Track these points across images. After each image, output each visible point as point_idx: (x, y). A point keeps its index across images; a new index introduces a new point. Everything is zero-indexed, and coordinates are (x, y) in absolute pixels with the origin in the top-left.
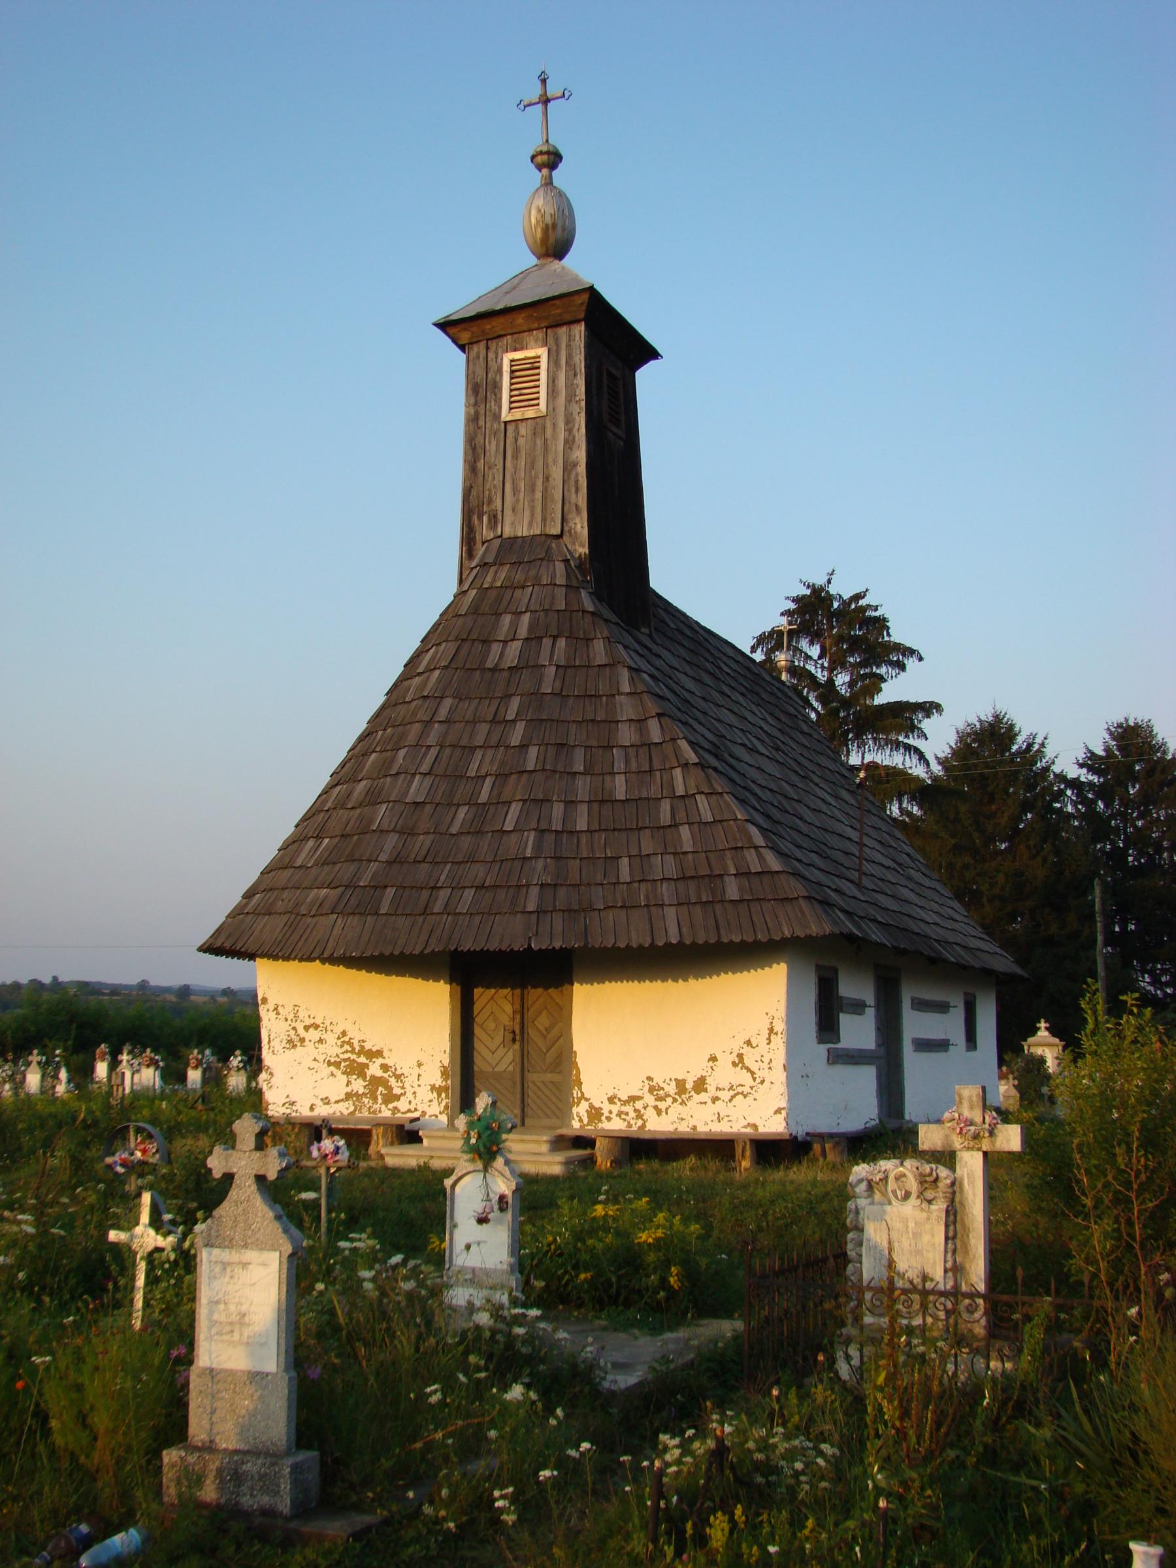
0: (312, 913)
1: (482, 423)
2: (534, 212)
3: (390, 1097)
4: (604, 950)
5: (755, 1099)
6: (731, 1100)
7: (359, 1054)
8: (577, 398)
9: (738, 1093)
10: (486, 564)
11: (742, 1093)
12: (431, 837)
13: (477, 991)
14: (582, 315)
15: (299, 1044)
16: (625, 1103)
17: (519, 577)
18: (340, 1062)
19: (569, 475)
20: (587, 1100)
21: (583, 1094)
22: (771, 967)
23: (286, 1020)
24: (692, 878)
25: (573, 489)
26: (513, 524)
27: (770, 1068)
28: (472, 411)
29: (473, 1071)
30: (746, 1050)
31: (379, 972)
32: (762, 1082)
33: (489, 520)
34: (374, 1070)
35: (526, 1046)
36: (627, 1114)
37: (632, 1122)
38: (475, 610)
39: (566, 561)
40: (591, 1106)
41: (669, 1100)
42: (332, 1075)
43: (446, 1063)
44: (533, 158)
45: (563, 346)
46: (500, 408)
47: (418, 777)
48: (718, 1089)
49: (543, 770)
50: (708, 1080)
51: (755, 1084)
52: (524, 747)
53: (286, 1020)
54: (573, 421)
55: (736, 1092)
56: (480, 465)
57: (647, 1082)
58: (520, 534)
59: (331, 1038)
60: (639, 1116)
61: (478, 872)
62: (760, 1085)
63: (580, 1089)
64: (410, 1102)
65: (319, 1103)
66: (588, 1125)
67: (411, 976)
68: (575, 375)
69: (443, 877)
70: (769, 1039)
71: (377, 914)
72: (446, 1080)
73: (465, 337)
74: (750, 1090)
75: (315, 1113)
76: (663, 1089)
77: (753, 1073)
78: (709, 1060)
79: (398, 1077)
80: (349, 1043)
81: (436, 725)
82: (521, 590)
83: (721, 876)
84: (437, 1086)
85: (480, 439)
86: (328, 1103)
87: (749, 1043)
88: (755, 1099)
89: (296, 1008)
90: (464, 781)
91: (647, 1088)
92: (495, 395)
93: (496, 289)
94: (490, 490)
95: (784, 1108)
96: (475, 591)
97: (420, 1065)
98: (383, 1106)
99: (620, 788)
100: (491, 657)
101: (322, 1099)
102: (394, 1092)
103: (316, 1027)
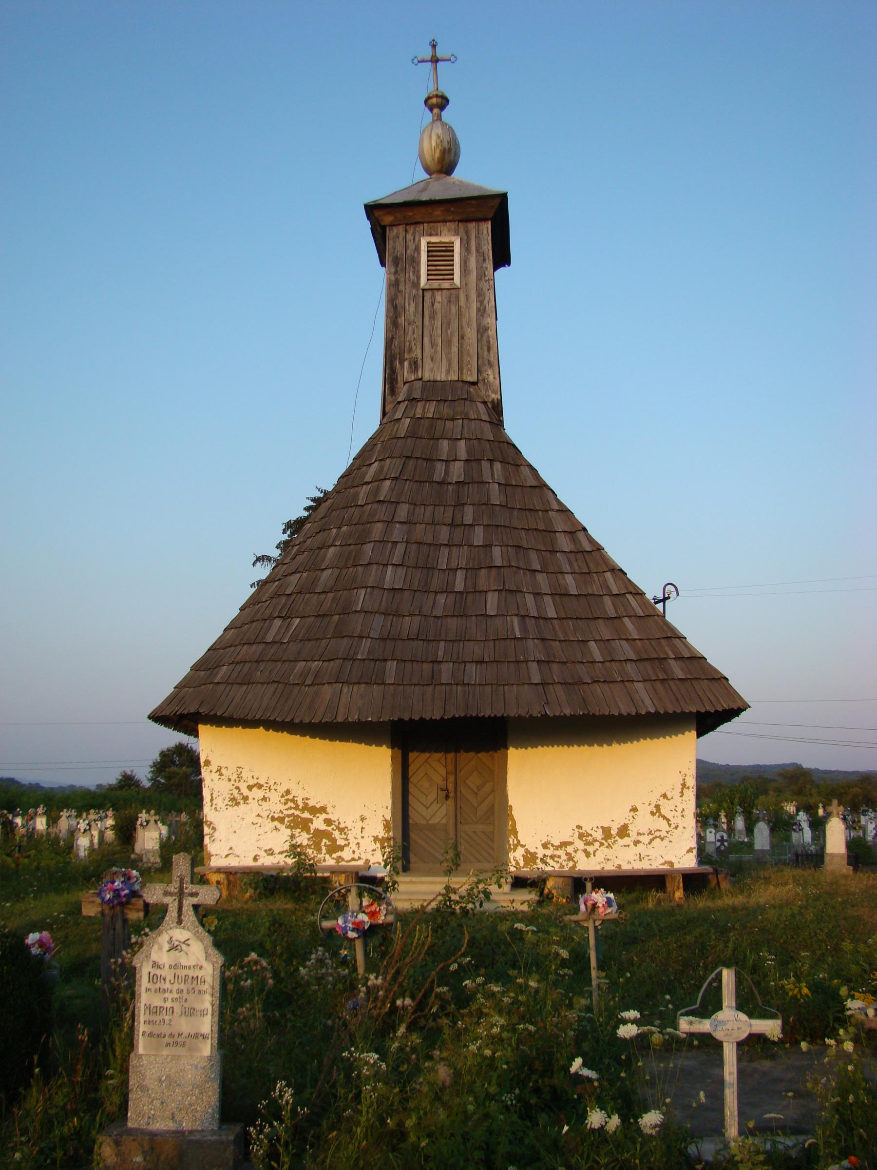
0: (308, 682)
1: (402, 287)
2: (434, 137)
3: (334, 848)
4: (611, 717)
5: (670, 841)
6: (650, 843)
7: (303, 810)
8: (487, 278)
9: (656, 837)
10: (414, 399)
11: (659, 837)
12: (417, 619)
13: (411, 755)
14: (491, 215)
15: (242, 802)
16: (557, 848)
17: (446, 410)
18: (284, 818)
19: (482, 336)
20: (523, 846)
21: (519, 841)
22: (684, 734)
23: (230, 780)
24: (646, 659)
25: (485, 348)
26: (432, 370)
27: (683, 816)
28: (393, 278)
29: (409, 824)
30: (663, 802)
31: (323, 737)
32: (676, 827)
33: (410, 364)
34: (318, 823)
35: (458, 802)
36: (559, 857)
37: (564, 863)
38: (412, 434)
39: (485, 403)
40: (527, 851)
41: (597, 844)
42: (276, 829)
43: (388, 817)
44: (426, 102)
45: (473, 237)
46: (419, 278)
47: (390, 567)
48: (639, 834)
49: (510, 566)
50: (631, 827)
51: (670, 829)
52: (488, 546)
53: (230, 780)
54: (484, 295)
55: (654, 836)
56: (401, 320)
57: (576, 830)
58: (439, 379)
59: (275, 797)
60: (570, 858)
61: (475, 649)
62: (674, 830)
63: (516, 837)
64: (354, 852)
65: (263, 854)
66: (523, 867)
67: (341, 741)
68: (484, 260)
69: (441, 653)
70: (682, 792)
71: (384, 684)
72: (388, 832)
73: (387, 219)
74: (666, 834)
75: (259, 863)
76: (591, 835)
77: (668, 820)
78: (631, 810)
79: (342, 830)
80: (293, 800)
81: (398, 525)
82: (451, 422)
83: (665, 659)
84: (380, 837)
85: (400, 301)
86: (272, 854)
87: (664, 796)
88: (670, 841)
89: (240, 770)
90: (436, 572)
91: (577, 835)
92: (414, 268)
93: (406, 189)
94: (410, 342)
95: (694, 848)
96: (408, 420)
97: (363, 819)
98: (327, 856)
99: (570, 583)
100: (437, 471)
101: (266, 851)
102: (338, 843)
103: (260, 786)
